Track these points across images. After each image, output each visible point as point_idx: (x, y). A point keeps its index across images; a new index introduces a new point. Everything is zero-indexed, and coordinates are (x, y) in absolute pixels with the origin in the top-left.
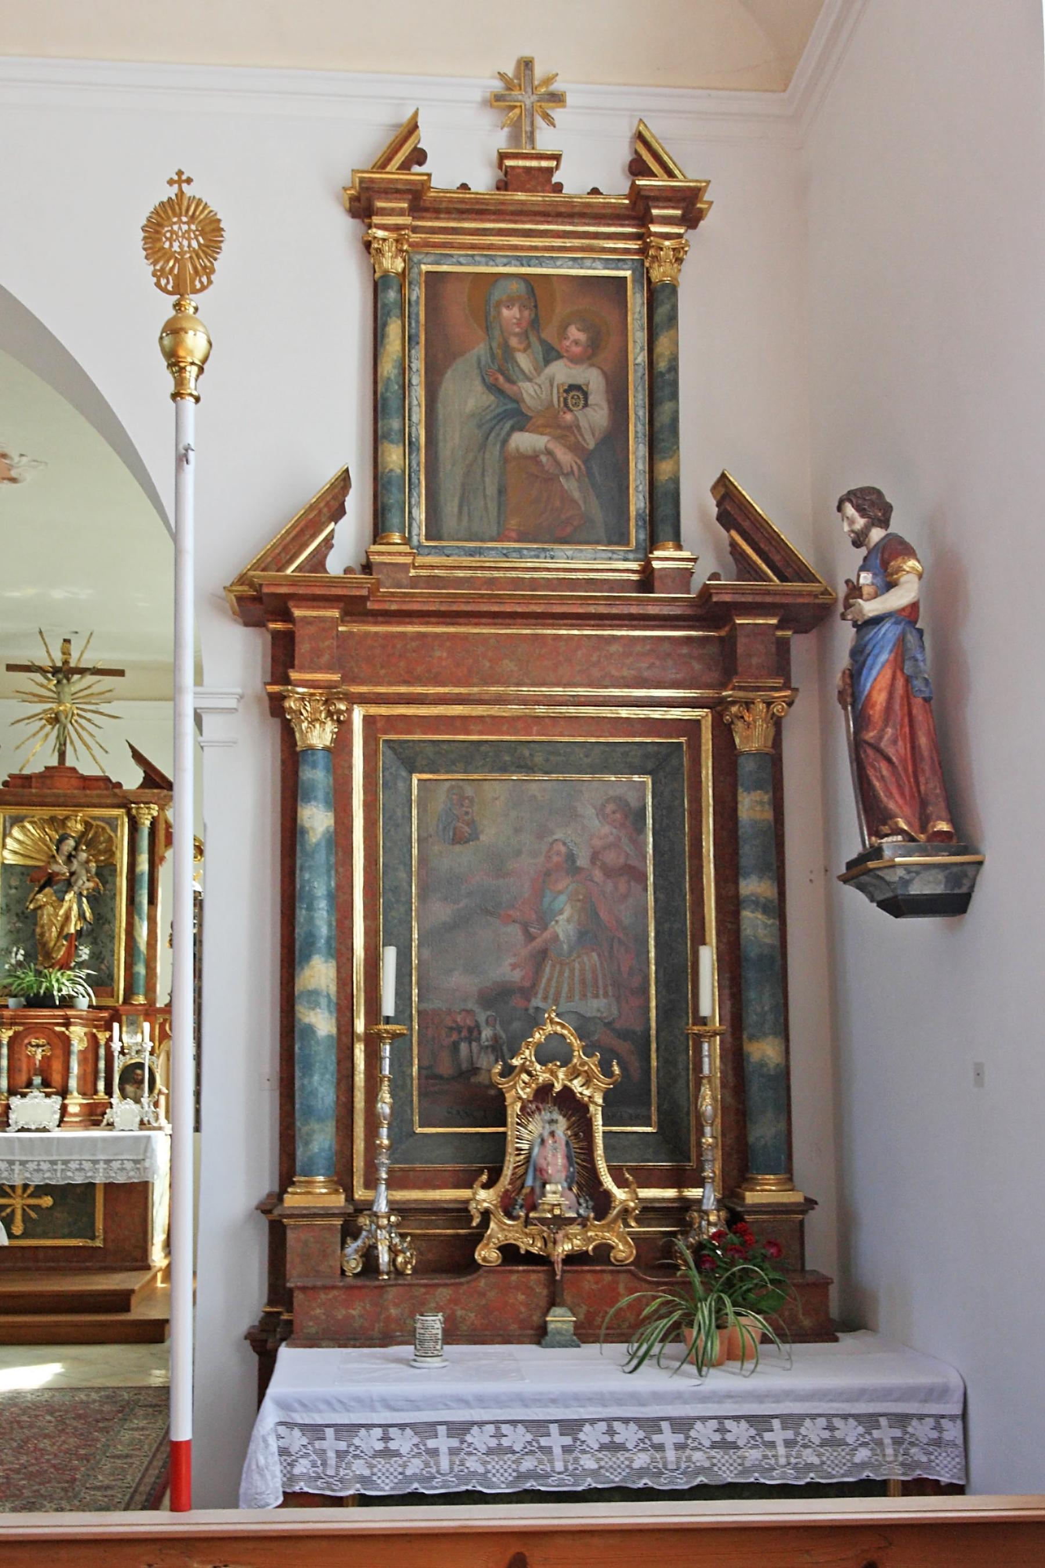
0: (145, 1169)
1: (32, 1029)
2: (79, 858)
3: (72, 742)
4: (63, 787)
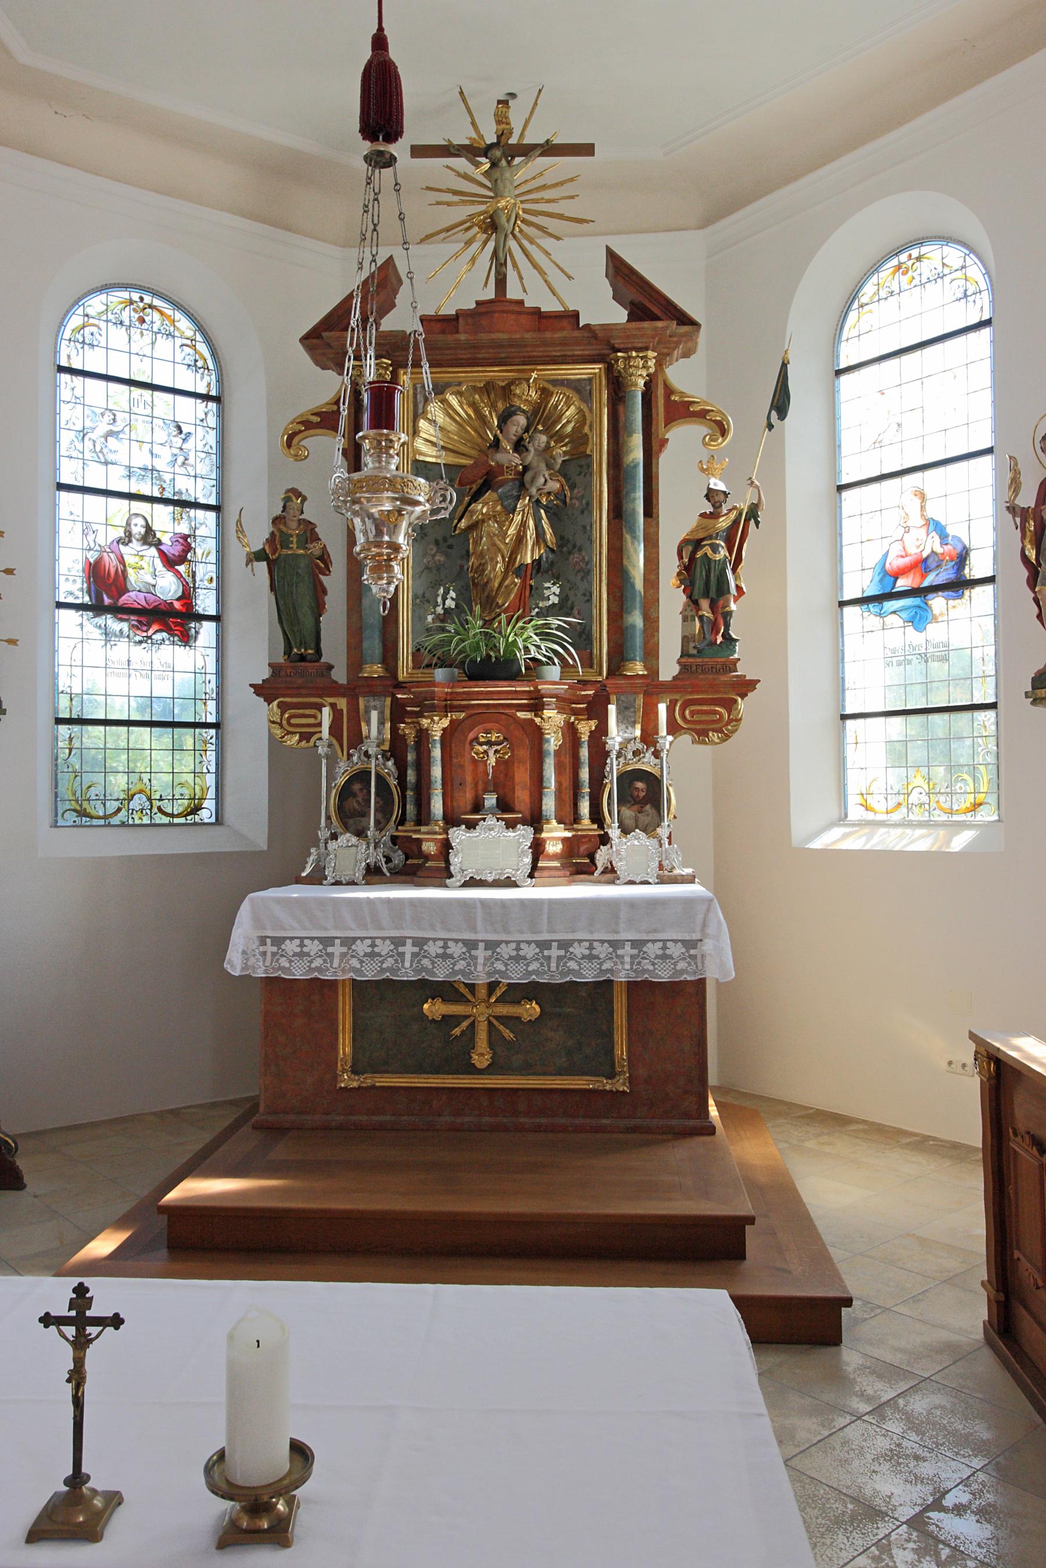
1: (480, 716)
3: (515, 265)
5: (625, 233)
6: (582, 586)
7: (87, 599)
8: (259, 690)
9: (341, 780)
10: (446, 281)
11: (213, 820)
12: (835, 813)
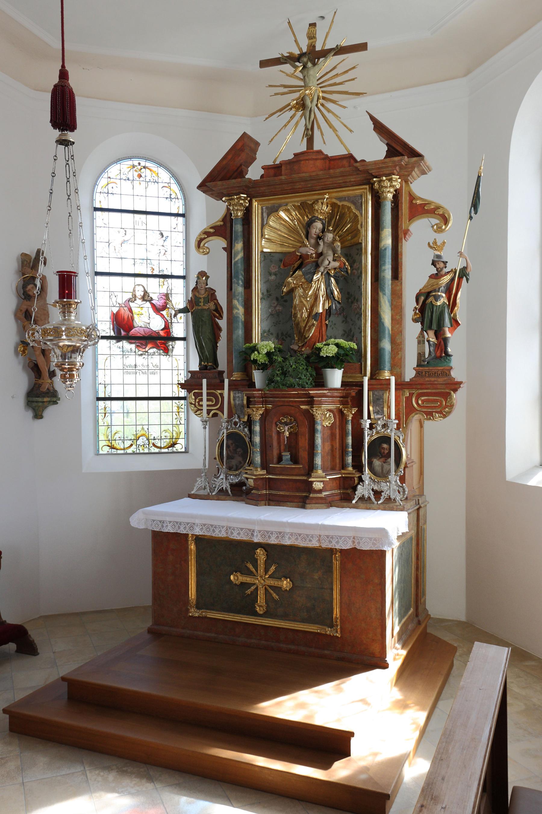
2: (326, 239)
3: (319, 127)
4: (310, 169)
5: (429, 84)
7: (112, 334)
10: (280, 144)
11: (183, 450)
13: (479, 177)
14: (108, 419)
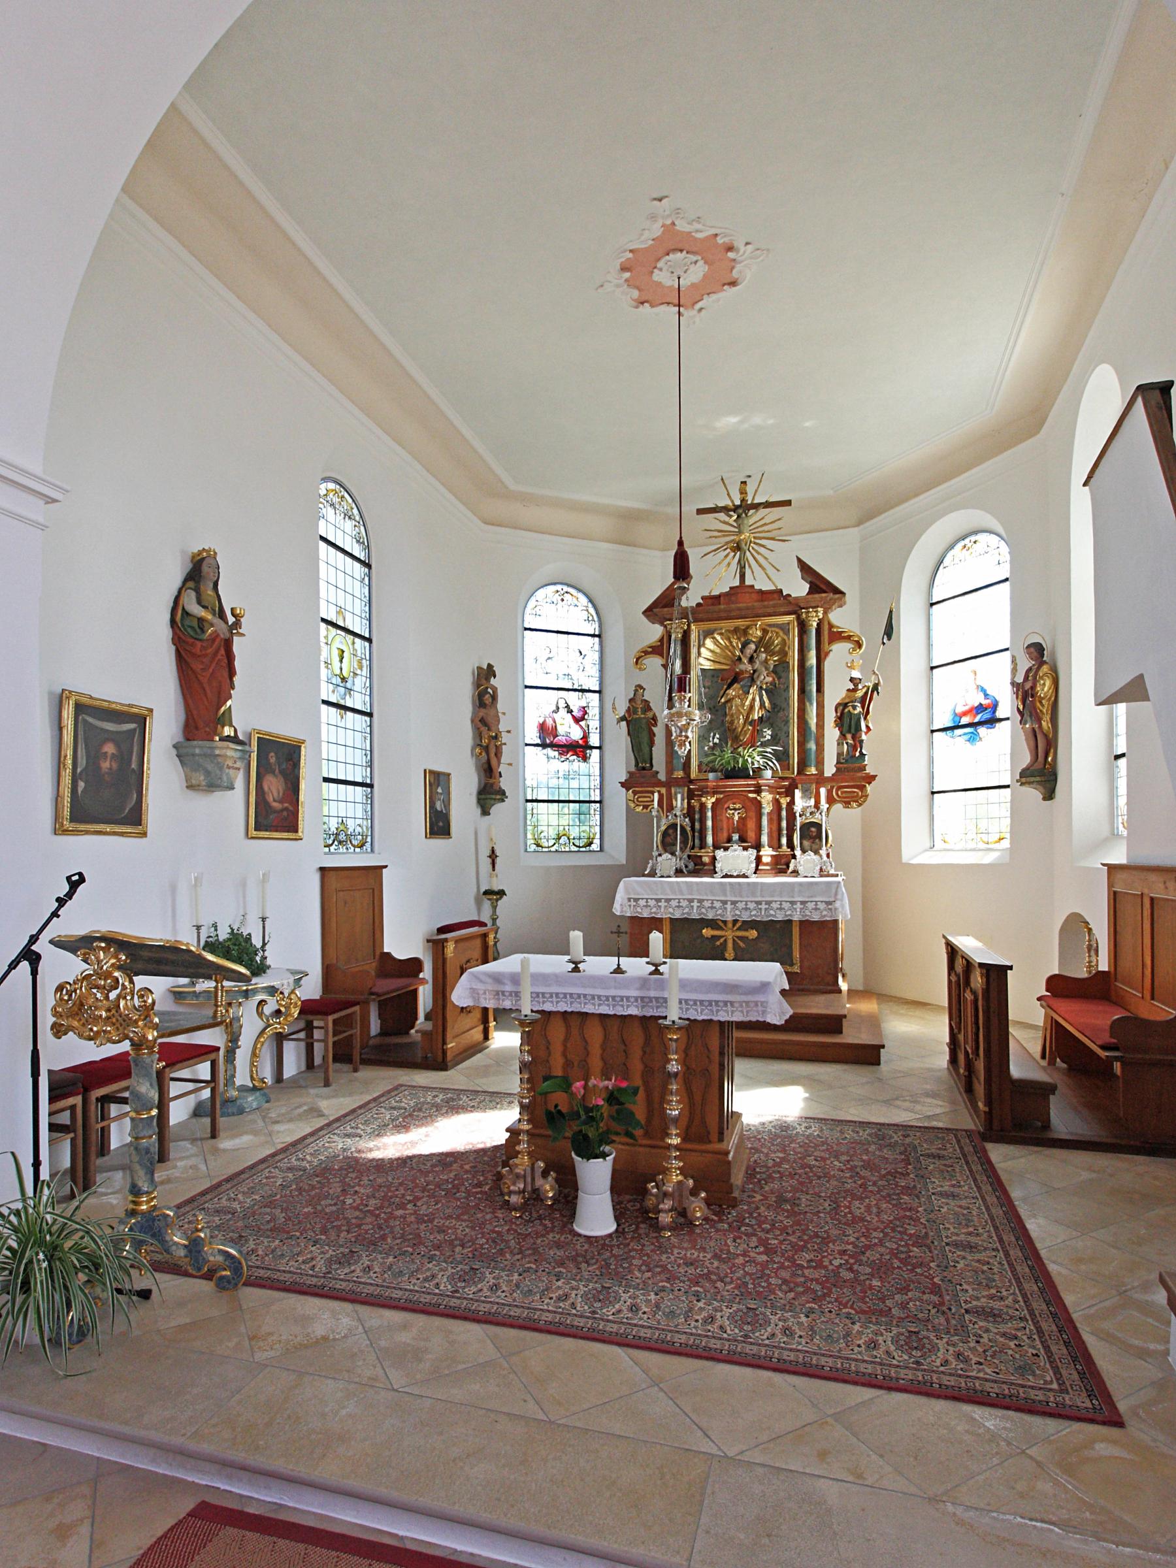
0: (836, 909)
4: (745, 602)
6: (785, 728)
8: (623, 784)
9: (663, 828)
10: (712, 576)
12: (928, 845)
13: (891, 612)
14: (534, 819)
